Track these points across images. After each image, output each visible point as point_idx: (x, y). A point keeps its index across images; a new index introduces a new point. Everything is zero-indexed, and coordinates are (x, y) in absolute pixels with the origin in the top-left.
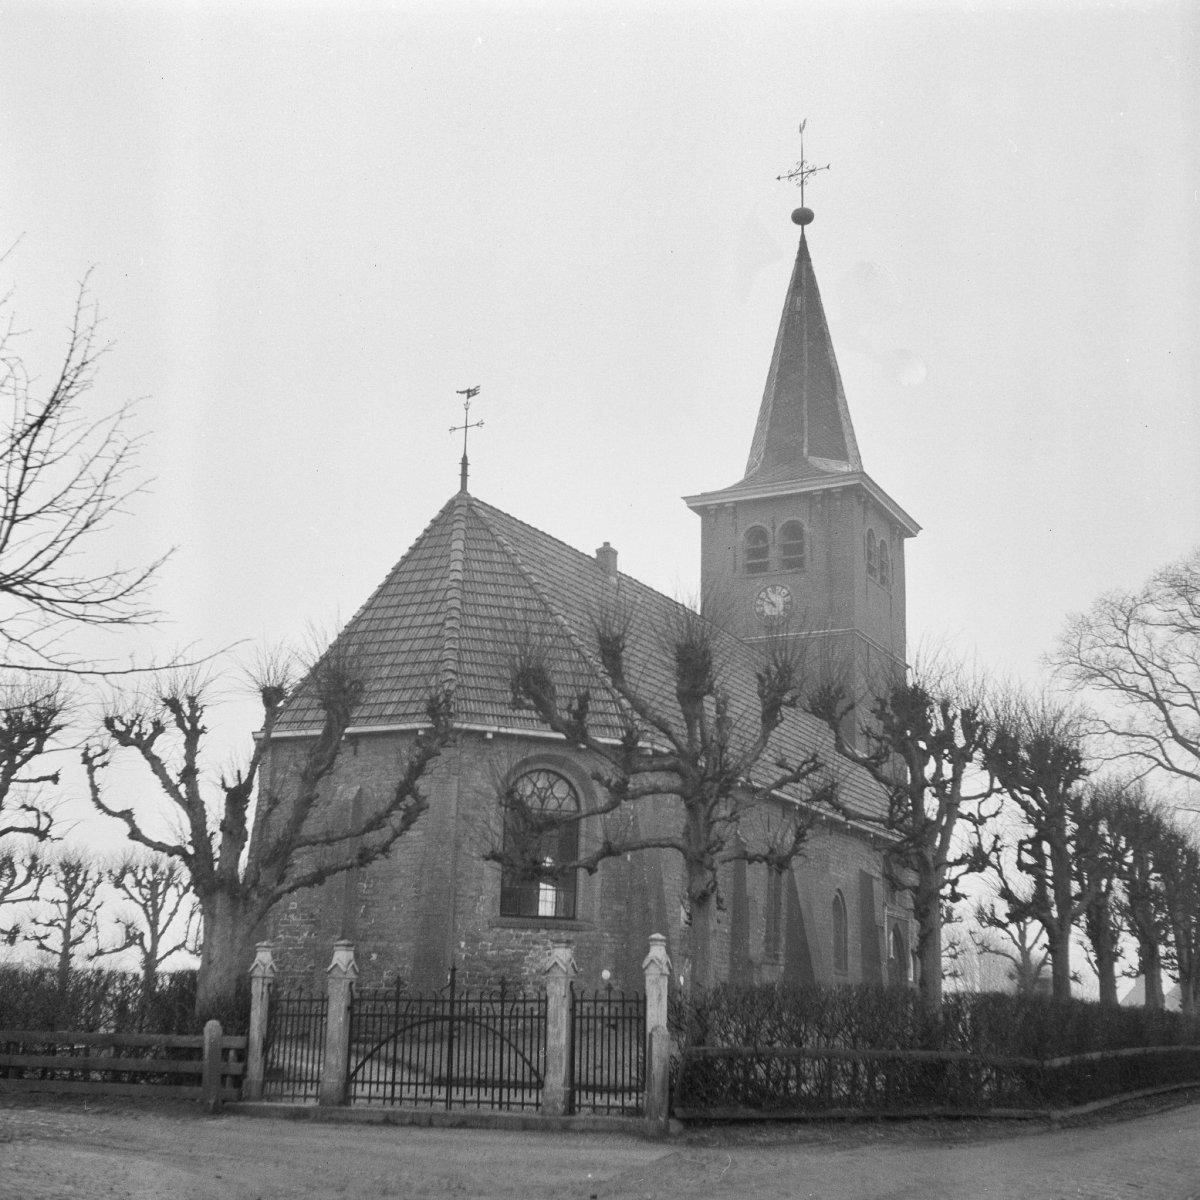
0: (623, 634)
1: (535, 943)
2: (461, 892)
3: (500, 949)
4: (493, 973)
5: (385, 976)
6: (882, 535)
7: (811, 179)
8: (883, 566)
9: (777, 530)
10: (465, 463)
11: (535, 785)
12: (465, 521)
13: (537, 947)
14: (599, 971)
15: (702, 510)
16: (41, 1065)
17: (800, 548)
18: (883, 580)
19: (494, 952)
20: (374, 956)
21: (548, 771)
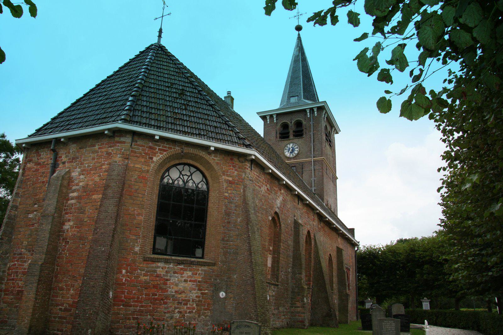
0: (222, 332)
1: (175, 273)
7: (300, 17)
10: (160, 31)
12: (158, 54)
15: (264, 118)
16: (355, 305)
21: (190, 165)
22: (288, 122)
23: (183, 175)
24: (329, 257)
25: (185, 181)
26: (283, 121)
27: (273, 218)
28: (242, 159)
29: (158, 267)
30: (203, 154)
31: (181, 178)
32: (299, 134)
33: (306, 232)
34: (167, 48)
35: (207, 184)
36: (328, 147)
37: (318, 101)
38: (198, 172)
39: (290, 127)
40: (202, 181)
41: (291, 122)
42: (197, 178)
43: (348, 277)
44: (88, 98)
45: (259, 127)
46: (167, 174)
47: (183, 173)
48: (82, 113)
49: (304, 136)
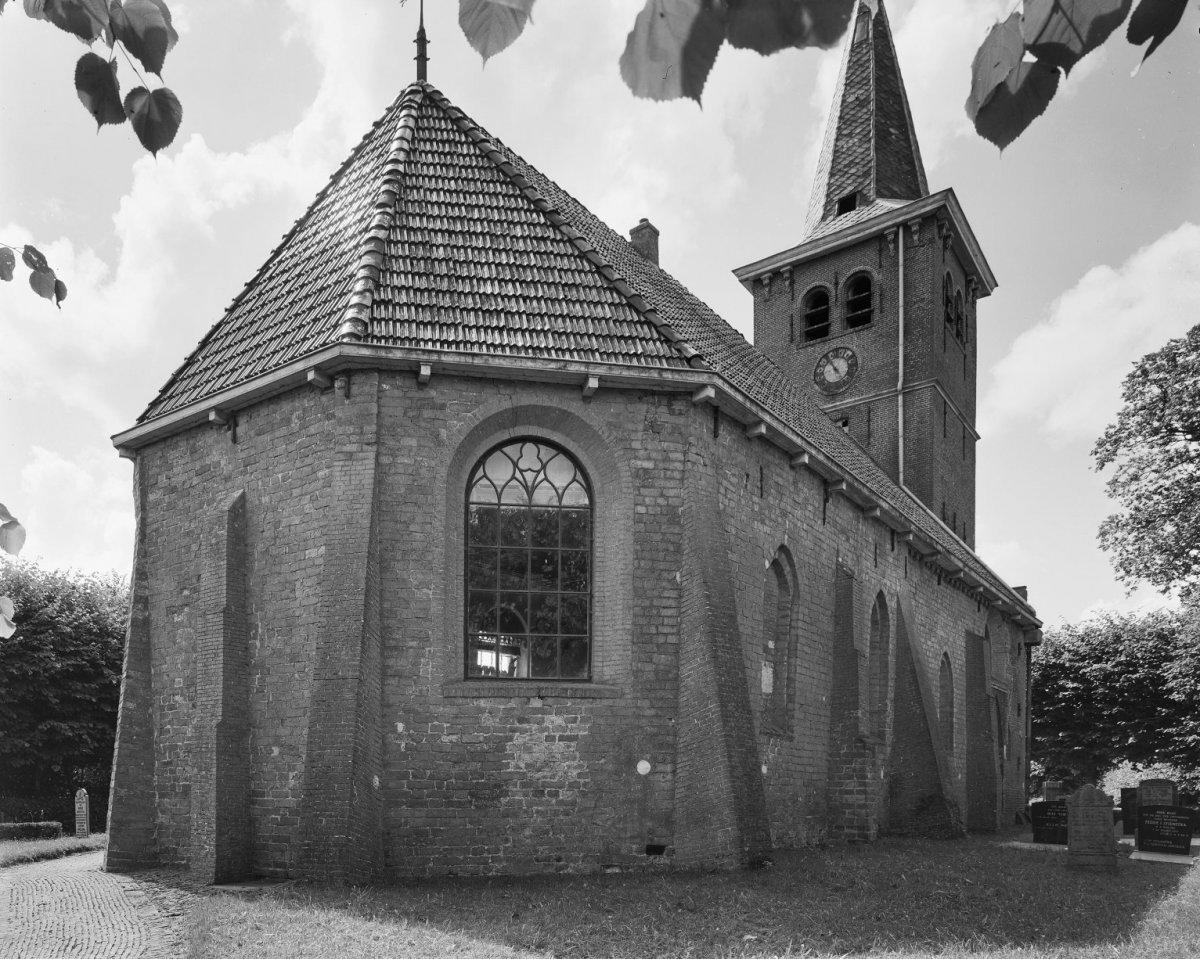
2: (393, 643)
3: (463, 732)
4: (455, 771)
5: (292, 782)
6: (958, 286)
8: (959, 318)
9: (840, 286)
10: (422, 40)
11: (515, 465)
12: (1025, 587)
13: (526, 726)
14: (632, 763)
17: (867, 302)
18: (959, 334)
19: (454, 738)
20: (276, 751)
21: (537, 441)
22: (828, 285)
23: (521, 471)
24: (943, 662)
25: (530, 484)
26: (813, 284)
27: (775, 563)
28: (678, 406)
29: (481, 710)
30: (573, 405)
31: (517, 480)
32: (860, 315)
33: (872, 599)
34: (445, 96)
35: (589, 489)
36: (512, 20)
37: (928, 193)
38: (561, 457)
39: (832, 300)
40: (574, 480)
41: (832, 280)
42: (560, 474)
43: (999, 713)
44: (257, 292)
45: (738, 310)
46: (480, 473)
47: (522, 465)
48: (249, 337)
49: (876, 317)
